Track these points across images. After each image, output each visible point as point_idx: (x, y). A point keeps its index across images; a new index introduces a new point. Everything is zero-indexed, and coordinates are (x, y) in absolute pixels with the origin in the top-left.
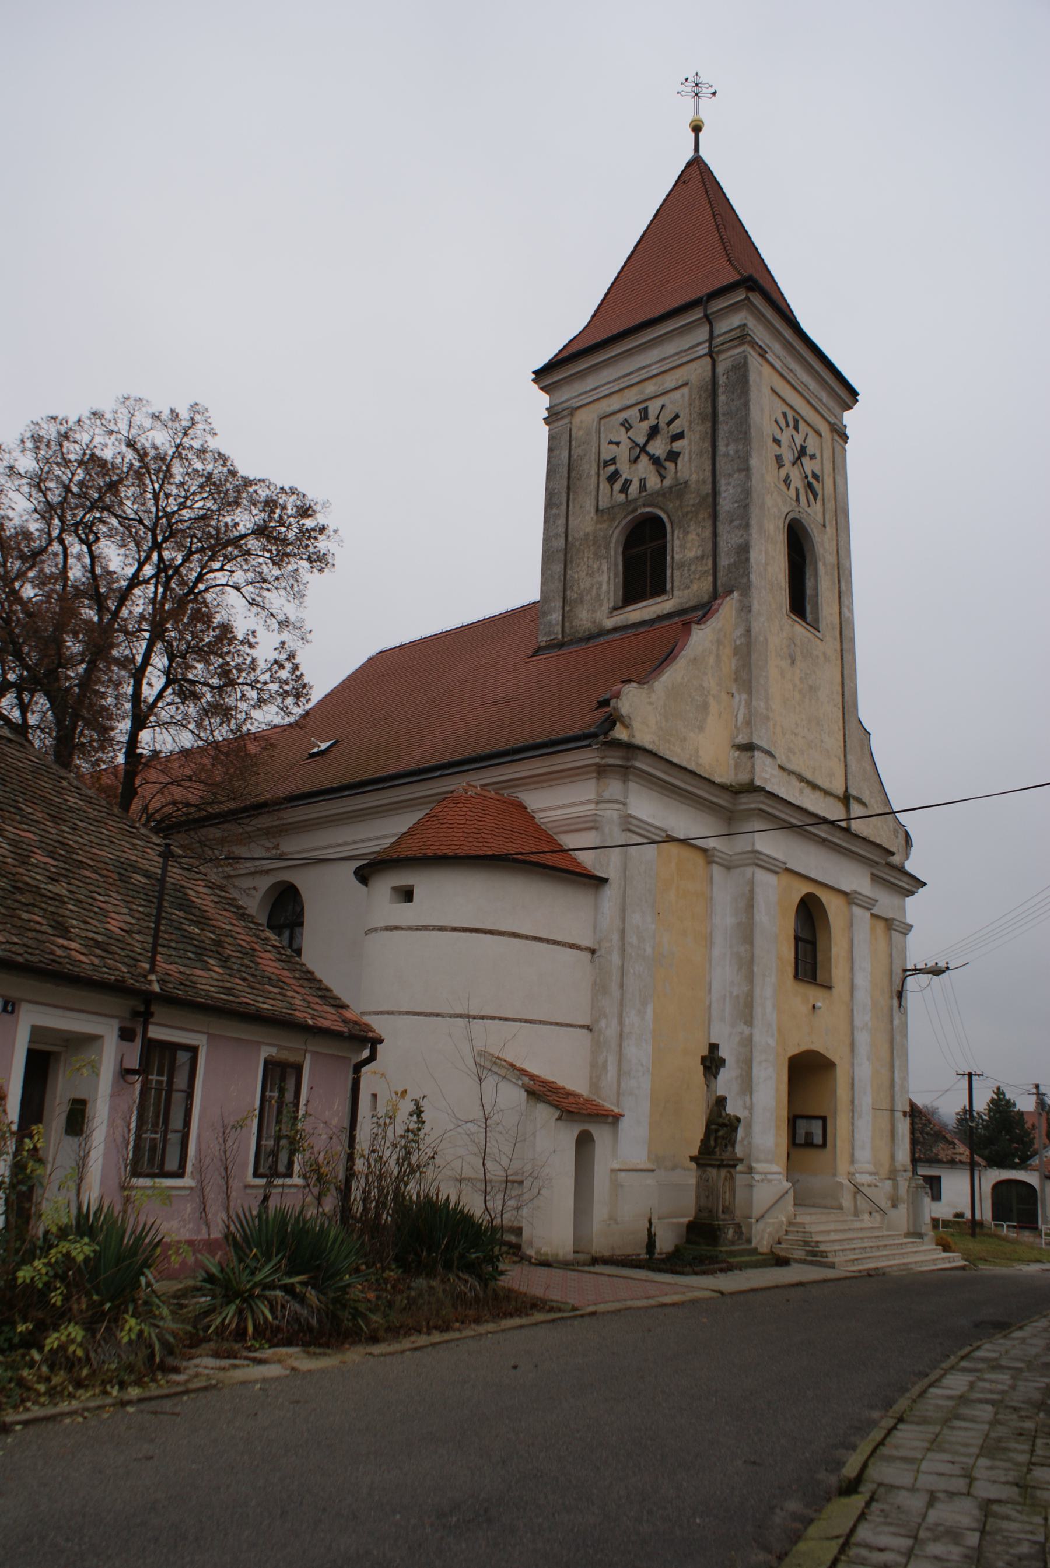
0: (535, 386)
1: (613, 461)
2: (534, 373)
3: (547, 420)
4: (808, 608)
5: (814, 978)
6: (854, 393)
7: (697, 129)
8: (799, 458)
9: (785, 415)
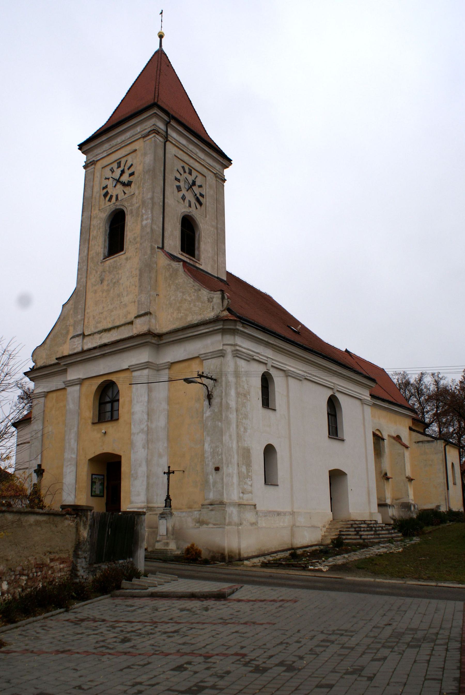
0: (80, 151)
1: (106, 187)
2: (78, 145)
3: (85, 167)
4: (196, 252)
5: (337, 435)
6: (230, 161)
7: (161, 36)
8: (191, 187)
9: (183, 167)
